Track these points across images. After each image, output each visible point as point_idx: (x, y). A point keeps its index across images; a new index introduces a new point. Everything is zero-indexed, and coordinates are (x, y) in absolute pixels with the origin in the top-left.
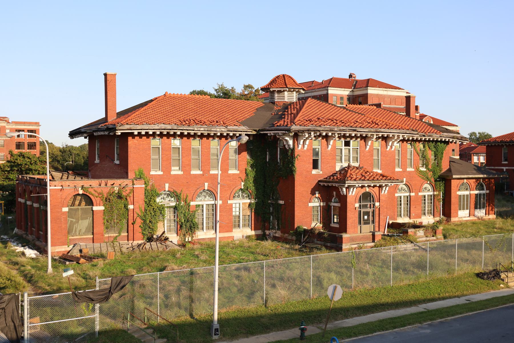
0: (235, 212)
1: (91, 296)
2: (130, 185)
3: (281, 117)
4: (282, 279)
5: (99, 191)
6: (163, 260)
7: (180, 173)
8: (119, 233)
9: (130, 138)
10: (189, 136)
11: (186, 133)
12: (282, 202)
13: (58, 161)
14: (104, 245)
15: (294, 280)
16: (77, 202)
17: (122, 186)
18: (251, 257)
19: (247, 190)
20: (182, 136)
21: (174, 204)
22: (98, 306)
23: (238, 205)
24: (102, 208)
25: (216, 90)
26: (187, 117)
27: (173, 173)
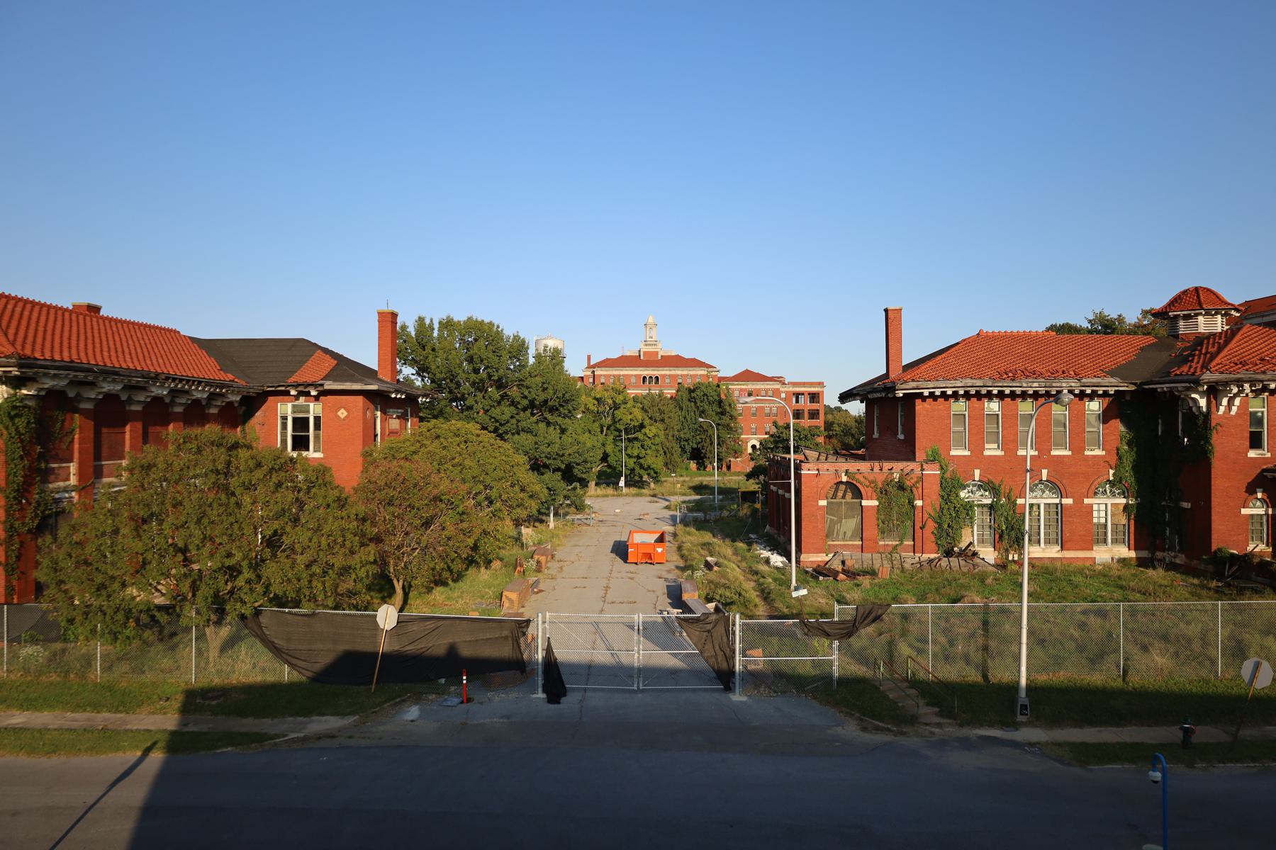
0: (1099, 516)
1: (826, 629)
2: (918, 471)
3: (1186, 360)
4: (1165, 638)
5: (871, 478)
6: (963, 586)
7: (1000, 453)
8: (901, 541)
9: (918, 402)
10: (1013, 395)
11: (1007, 391)
12: (1186, 505)
13: (853, 435)
14: (876, 556)
15: (1189, 641)
16: (840, 494)
17: (906, 471)
18: (1118, 594)
19: (1120, 482)
20: (1001, 395)
21: (989, 501)
22: (836, 643)
23: (1103, 507)
24: (876, 503)
25: (1090, 321)
26: (1004, 368)
27: (987, 453)
